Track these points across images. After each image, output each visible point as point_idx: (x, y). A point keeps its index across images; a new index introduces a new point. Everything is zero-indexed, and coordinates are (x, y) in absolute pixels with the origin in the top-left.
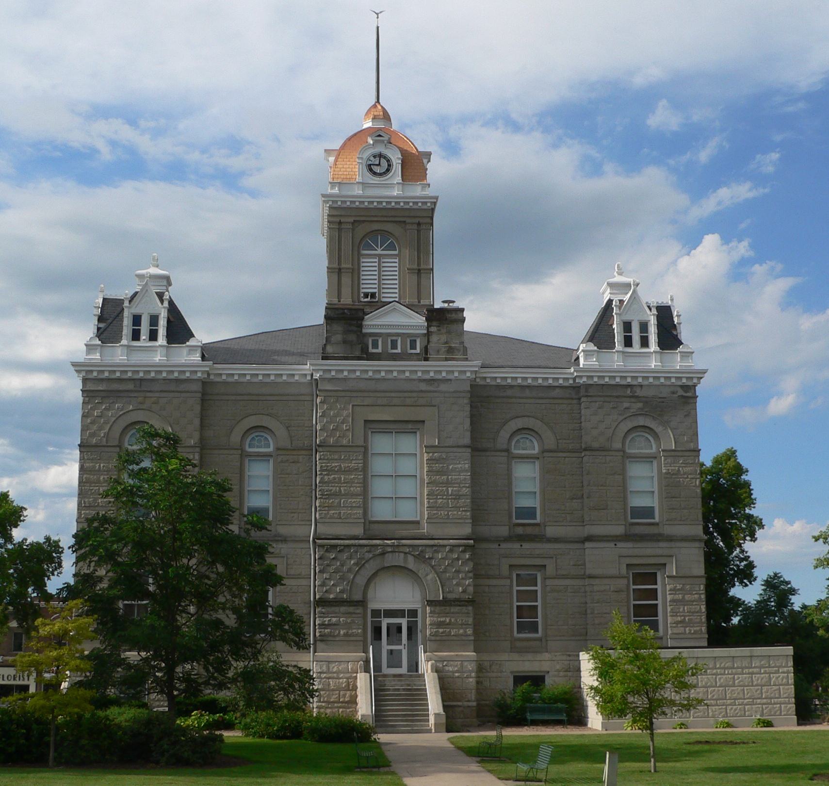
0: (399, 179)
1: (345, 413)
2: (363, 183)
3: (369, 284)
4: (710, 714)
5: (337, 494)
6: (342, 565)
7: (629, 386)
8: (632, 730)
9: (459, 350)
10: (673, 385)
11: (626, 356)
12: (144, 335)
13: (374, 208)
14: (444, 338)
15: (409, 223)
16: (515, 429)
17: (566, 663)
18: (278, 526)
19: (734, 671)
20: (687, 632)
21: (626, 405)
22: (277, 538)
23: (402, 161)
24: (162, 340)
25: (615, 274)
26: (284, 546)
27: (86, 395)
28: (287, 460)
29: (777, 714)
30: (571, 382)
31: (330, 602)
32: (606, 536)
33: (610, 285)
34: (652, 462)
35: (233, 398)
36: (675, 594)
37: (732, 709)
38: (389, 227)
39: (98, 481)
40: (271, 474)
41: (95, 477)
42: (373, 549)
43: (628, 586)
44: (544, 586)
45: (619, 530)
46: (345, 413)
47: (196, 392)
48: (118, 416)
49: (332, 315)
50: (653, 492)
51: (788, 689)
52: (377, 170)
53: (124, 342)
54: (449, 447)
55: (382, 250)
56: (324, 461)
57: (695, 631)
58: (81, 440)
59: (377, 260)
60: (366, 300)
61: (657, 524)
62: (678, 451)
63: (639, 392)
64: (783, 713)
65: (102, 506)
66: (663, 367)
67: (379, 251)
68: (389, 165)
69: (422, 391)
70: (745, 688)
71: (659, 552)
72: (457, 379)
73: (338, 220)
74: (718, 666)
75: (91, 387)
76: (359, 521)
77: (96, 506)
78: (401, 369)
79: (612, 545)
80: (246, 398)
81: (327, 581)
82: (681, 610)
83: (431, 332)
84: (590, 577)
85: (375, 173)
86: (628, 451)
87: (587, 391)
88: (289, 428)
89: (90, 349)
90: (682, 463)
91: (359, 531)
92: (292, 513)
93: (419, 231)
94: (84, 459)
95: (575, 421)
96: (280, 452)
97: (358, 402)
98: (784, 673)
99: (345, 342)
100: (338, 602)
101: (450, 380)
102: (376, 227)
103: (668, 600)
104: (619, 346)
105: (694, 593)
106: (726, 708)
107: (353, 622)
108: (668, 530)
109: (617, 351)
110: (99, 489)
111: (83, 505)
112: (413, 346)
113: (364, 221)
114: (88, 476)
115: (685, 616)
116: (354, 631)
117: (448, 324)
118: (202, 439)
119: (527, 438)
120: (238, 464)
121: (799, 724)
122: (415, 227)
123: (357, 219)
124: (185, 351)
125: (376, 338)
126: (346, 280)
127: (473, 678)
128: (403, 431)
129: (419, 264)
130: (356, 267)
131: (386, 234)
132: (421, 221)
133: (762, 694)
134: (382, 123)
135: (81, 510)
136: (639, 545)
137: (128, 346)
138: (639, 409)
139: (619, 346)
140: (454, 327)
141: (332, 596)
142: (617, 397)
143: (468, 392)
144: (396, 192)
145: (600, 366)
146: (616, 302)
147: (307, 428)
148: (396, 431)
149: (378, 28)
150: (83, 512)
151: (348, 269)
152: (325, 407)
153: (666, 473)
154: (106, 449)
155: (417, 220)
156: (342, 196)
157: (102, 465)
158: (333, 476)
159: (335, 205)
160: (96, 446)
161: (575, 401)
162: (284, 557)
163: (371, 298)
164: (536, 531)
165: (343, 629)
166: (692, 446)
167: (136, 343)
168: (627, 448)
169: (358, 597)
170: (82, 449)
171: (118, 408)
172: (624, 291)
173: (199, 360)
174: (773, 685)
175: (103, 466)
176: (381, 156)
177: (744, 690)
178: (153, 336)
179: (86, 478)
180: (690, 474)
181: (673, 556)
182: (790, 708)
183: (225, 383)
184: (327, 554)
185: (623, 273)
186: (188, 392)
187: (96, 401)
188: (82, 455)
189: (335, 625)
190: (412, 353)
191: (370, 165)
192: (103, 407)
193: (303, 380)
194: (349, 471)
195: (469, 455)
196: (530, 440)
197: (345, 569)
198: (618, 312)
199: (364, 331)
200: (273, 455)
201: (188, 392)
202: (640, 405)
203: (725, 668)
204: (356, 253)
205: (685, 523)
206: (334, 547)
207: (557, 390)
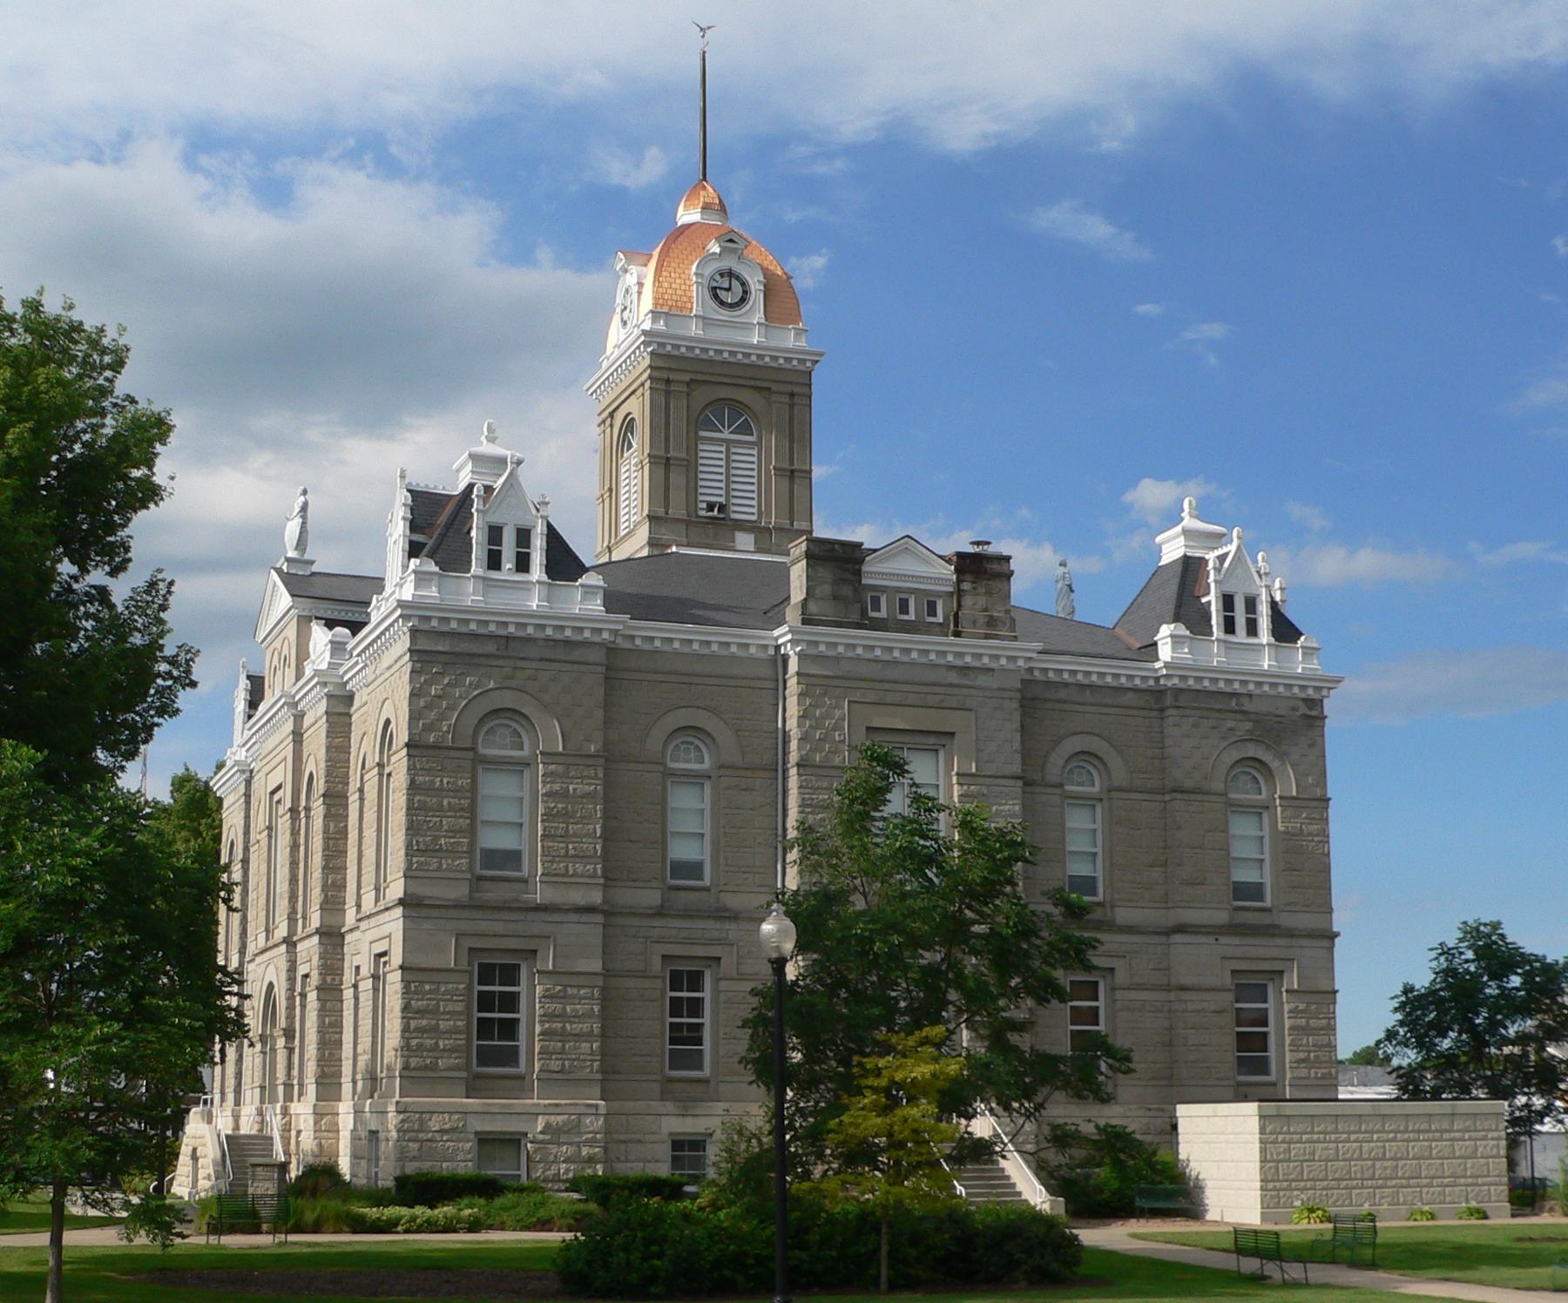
0: (758, 316)
1: (837, 713)
2: (704, 318)
3: (711, 489)
4: (1401, 1200)
7: (1234, 695)
8: (1309, 1223)
9: (1004, 623)
10: (1294, 698)
11: (488, 585)
13: (723, 362)
14: (982, 601)
15: (777, 393)
17: (1144, 1121)
18: (723, 894)
19: (1431, 1135)
20: (1313, 1075)
21: (1230, 724)
22: (723, 914)
23: (765, 286)
25: (483, 438)
26: (733, 926)
27: (416, 659)
28: (737, 786)
29: (1346, 1203)
30: (1151, 682)
32: (1205, 926)
33: (471, 456)
34: (522, 772)
35: (650, 677)
36: (1296, 1018)
37: (1428, 1192)
38: (744, 396)
39: (440, 808)
40: (707, 805)
41: (434, 800)
43: (470, 987)
44: (716, 992)
45: (1221, 917)
46: (837, 713)
48: (470, 697)
49: (817, 551)
50: (702, 835)
52: (722, 294)
54: (990, 777)
55: (731, 433)
56: (807, 791)
57: (1322, 1074)
58: (409, 735)
59: (723, 449)
60: (710, 514)
61: (707, 889)
62: (1303, 799)
63: (1248, 706)
64: (1493, 1199)
65: (447, 851)
66: (1279, 667)
67: (726, 435)
68: (745, 292)
69: (951, 685)
70: (1445, 1161)
71: (1275, 952)
72: (1003, 670)
73: (664, 375)
74: (1410, 1128)
75: (423, 644)
77: (436, 851)
78: (995, 652)
79: (1211, 940)
82: (1304, 1042)
83: (963, 590)
84: (1183, 988)
85: (722, 303)
86: (482, 751)
87: (1176, 700)
88: (740, 733)
89: (420, 579)
90: (1305, 818)
92: (744, 872)
93: (792, 406)
94: (414, 767)
95: (1155, 745)
96: (722, 772)
97: (857, 696)
98: (1492, 1139)
101: (993, 670)
102: (723, 393)
103: (1287, 1027)
104: (477, 568)
105: (1321, 1016)
106: (1421, 1192)
108: (1287, 920)
109: (473, 577)
110: (441, 821)
111: (415, 848)
112: (932, 611)
113: (705, 382)
114: (422, 798)
115: (1309, 1052)
117: (989, 580)
118: (607, 744)
119: (1084, 768)
121: (1513, 1216)
123: (699, 377)
125: (877, 594)
126: (677, 479)
127: (1031, 1143)
128: (919, 747)
131: (737, 408)
132: (796, 390)
133: (1466, 1169)
134: (717, 217)
135: (412, 856)
136: (1250, 941)
138: (1248, 731)
139: (477, 568)
140: (996, 585)
142: (1219, 711)
143: (1019, 691)
145: (1194, 661)
146: (479, 490)
147: (766, 735)
148: (909, 746)
149: (704, 52)
150: (414, 860)
151: (683, 460)
152: (808, 703)
153: (1284, 832)
154: (453, 753)
155: (789, 388)
156: (706, 341)
157: (445, 780)
158: (820, 816)
159: (661, 351)
160: (435, 747)
161: (1155, 714)
162: (733, 945)
163: (719, 511)
164: (1265, 919)
166: (1318, 792)
167: (494, 575)
168: (480, 746)
170: (413, 752)
171: (470, 684)
172: (496, 472)
173: (601, 611)
175: (448, 783)
176: (730, 274)
177: (1443, 1164)
178: (523, 564)
179: (419, 801)
181: (1293, 960)
182: (1502, 1191)
183: (639, 652)
185: (496, 438)
187: (434, 670)
188: (411, 763)
190: (932, 623)
191: (715, 288)
192: (446, 681)
193: (762, 655)
195: (1019, 790)
196: (1089, 771)
198: (481, 507)
199: (864, 581)
200: (711, 774)
202: (1249, 725)
203: (1419, 1131)
205: (1308, 909)
207: (1130, 695)
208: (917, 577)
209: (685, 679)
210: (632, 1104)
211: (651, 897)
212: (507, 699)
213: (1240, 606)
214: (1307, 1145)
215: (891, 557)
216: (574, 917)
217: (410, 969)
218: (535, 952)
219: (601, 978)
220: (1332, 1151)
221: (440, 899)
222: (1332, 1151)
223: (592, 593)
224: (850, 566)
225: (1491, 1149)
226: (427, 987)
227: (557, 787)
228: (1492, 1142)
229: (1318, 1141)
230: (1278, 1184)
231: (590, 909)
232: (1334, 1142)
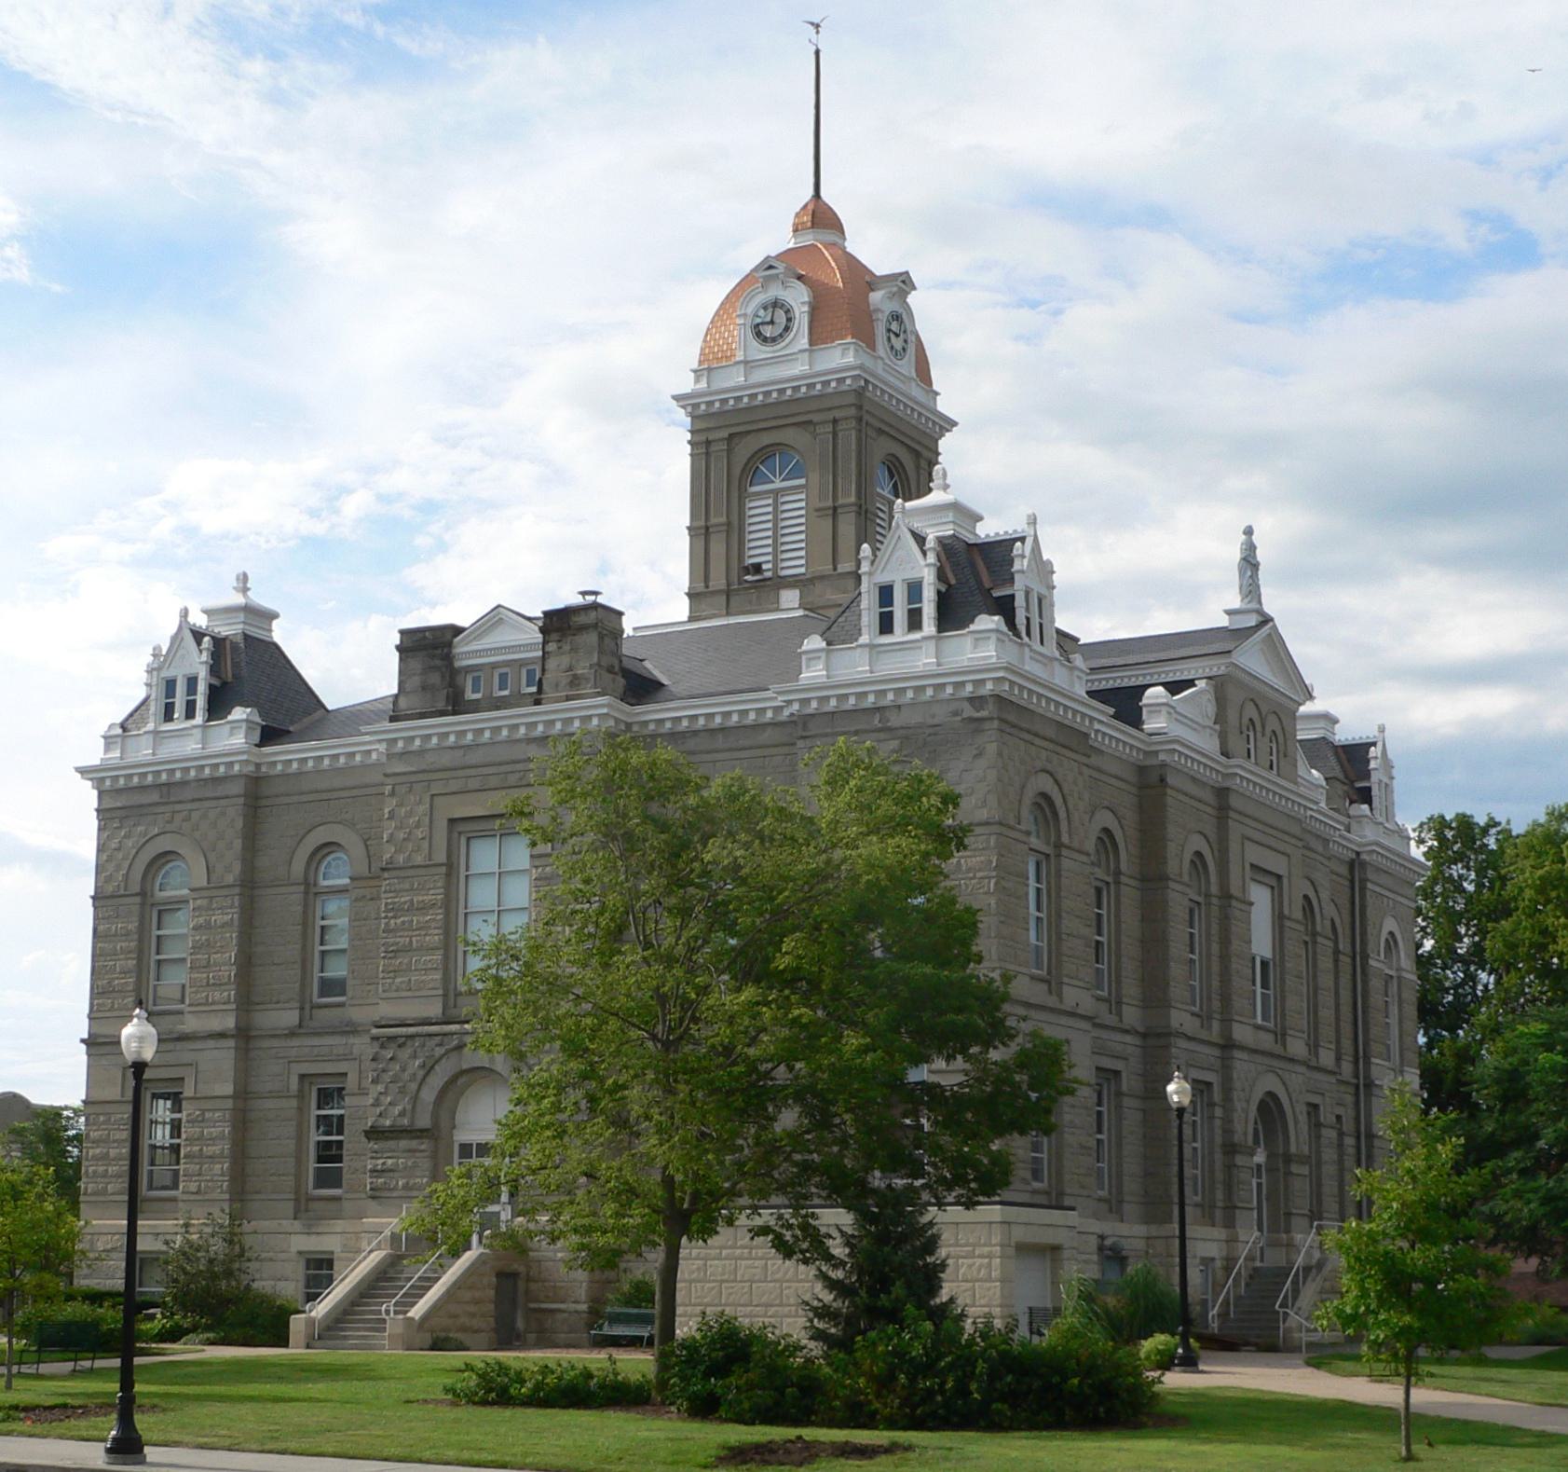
0: (803, 342)
5: (407, 949)
6: (403, 1069)
9: (587, 680)
14: (565, 660)
24: (929, 627)
31: (383, 1132)
42: (446, 1039)
51: (989, 1289)
53: (864, 639)
63: (895, 720)
67: (778, 484)
76: (435, 992)
80: (311, 797)
81: (382, 1098)
85: (765, 340)
91: (435, 1010)
98: (981, 1256)
99: (424, 688)
100: (395, 1133)
102: (767, 439)
107: (415, 1166)
113: (749, 432)
116: (418, 1180)
120: (300, 909)
124: (969, 641)
129: (835, 498)
134: (811, 237)
137: (871, 646)
141: (388, 1123)
144: (799, 368)
149: (817, 53)
155: (830, 416)
165: (403, 1177)
169: (424, 1121)
176: (776, 304)
178: (915, 621)
180: (980, 870)
183: (283, 776)
184: (383, 1052)
186: (227, 797)
189: (391, 1171)
191: (758, 325)
194: (423, 908)
197: (406, 1076)
199: (457, 664)
201: (227, 797)
202: (894, 744)
204: (735, 494)
206: (391, 1038)
207: (769, 731)
208: (509, 647)
209: (325, 796)
210: (267, 1223)
211: (290, 1018)
212: (164, 844)
213: (899, 596)
214: (727, 1262)
215: (479, 637)
216: (211, 1043)
217: (93, 1103)
218: (182, 1079)
219: (231, 1101)
220: (758, 1270)
221: (106, 1036)
222: (758, 1270)
223: (814, 658)
224: (439, 651)
225: (979, 1270)
226: (102, 1118)
227: (201, 920)
228: (978, 1261)
229: (741, 1258)
230: (689, 1309)
231: (222, 1035)
232: (761, 1259)
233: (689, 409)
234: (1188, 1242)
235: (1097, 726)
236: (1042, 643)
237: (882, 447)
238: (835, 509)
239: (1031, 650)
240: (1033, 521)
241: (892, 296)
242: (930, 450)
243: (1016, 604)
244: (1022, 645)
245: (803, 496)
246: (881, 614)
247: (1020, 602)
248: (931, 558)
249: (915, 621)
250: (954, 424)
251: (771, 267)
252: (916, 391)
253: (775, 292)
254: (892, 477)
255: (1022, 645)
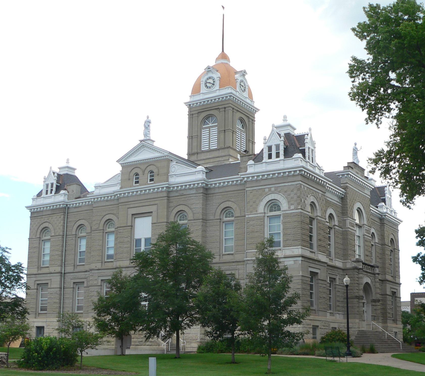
12: (274, 155)
16: (43, 228)
24: (282, 157)
38: (211, 112)
47: (165, 197)
67: (210, 125)
122: (224, 109)
126: (195, 140)
130: (199, 134)
144: (218, 93)
155: (224, 106)
174: (146, 357)
178: (278, 155)
233: (188, 106)
234: (346, 322)
235: (327, 185)
236: (312, 162)
237: (238, 115)
238: (225, 131)
239: (310, 164)
240: (310, 129)
241: (241, 76)
242: (253, 117)
243: (306, 151)
244: (306, 162)
245: (217, 128)
246: (269, 154)
247: (307, 151)
248: (282, 138)
249: (278, 155)
250: (259, 110)
251: (209, 68)
252: (248, 101)
253: (210, 75)
254: (242, 123)
255: (306, 162)
